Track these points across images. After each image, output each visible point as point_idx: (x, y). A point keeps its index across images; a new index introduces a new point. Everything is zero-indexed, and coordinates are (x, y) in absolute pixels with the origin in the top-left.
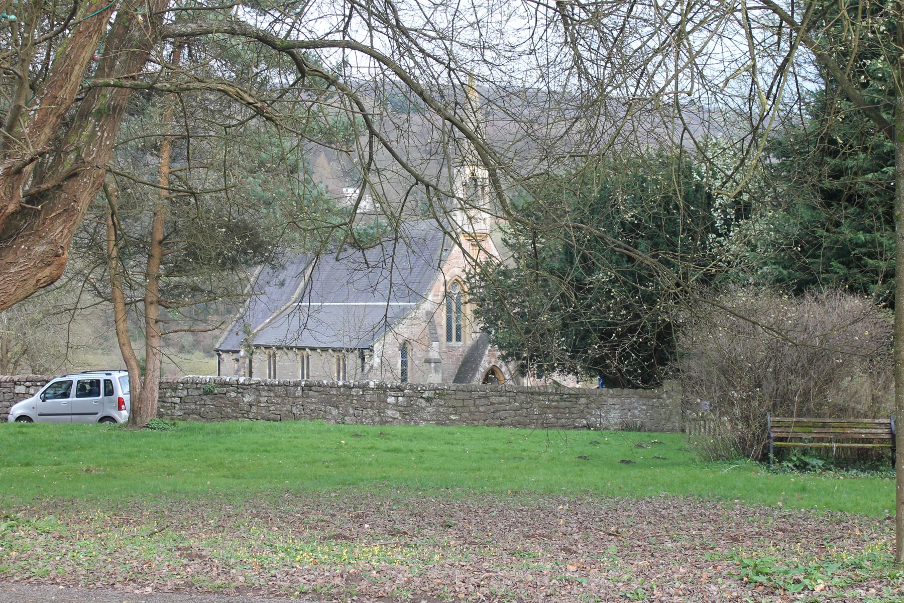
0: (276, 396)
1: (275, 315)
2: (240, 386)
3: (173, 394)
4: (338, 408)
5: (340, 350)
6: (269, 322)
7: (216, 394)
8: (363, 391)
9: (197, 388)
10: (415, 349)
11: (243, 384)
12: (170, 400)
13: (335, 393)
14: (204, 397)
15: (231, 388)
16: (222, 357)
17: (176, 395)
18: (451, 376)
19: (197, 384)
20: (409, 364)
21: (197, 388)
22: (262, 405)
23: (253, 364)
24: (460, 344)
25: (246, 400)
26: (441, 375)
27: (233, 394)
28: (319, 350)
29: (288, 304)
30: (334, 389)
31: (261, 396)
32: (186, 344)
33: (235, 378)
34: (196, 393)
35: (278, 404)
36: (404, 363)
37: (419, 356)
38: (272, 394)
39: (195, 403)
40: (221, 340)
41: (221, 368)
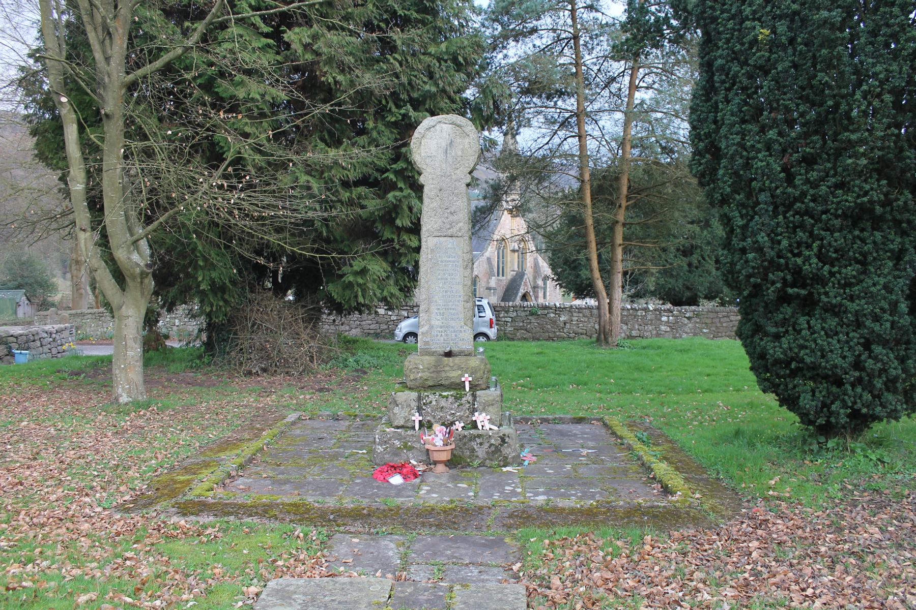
4: (627, 324)
27: (552, 315)
34: (523, 314)
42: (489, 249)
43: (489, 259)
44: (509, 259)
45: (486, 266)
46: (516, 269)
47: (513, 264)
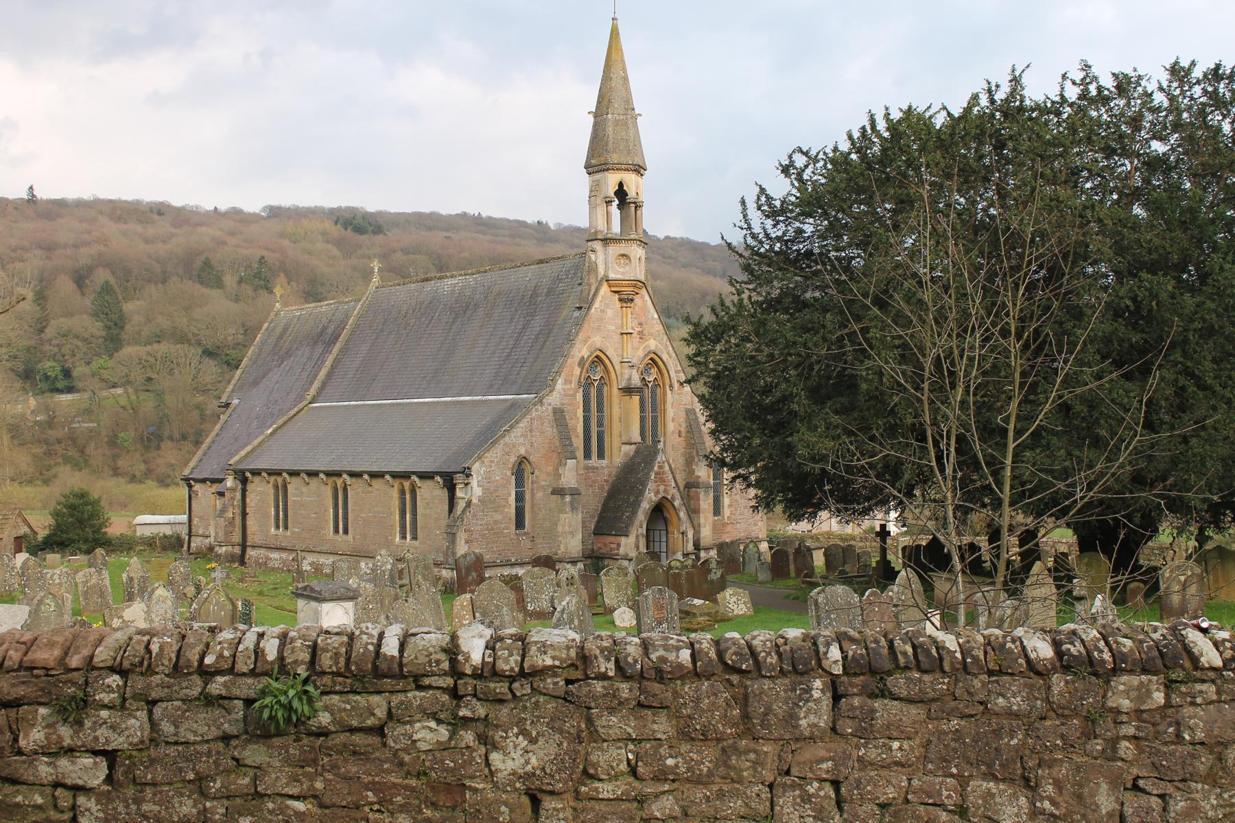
0: (685, 735)
1: (280, 422)
2: (466, 686)
3: (65, 733)
4: (1029, 784)
5: (405, 475)
6: (272, 434)
7: (323, 733)
8: (1169, 685)
9: (209, 701)
10: (537, 472)
11: (488, 672)
12: (44, 770)
13: (1017, 703)
14: (254, 754)
15: (415, 696)
16: (194, 489)
17: (86, 736)
18: (593, 516)
19: (207, 673)
20: (528, 497)
21: (209, 701)
22: (606, 790)
23: (248, 500)
24: (604, 462)
25: (507, 762)
26: (580, 516)
27: (428, 734)
28: (322, 475)
29: (301, 405)
30: (1015, 685)
31: (595, 736)
32: (137, 474)
33: (432, 639)
34: (200, 726)
35: (699, 781)
36: (520, 498)
37: (543, 483)
38: (662, 726)
39: (200, 785)
40: (192, 464)
41: (194, 505)
42: (559, 385)
43: (559, 415)
44: (616, 411)
45: (551, 431)
46: (636, 437)
47: (627, 426)
